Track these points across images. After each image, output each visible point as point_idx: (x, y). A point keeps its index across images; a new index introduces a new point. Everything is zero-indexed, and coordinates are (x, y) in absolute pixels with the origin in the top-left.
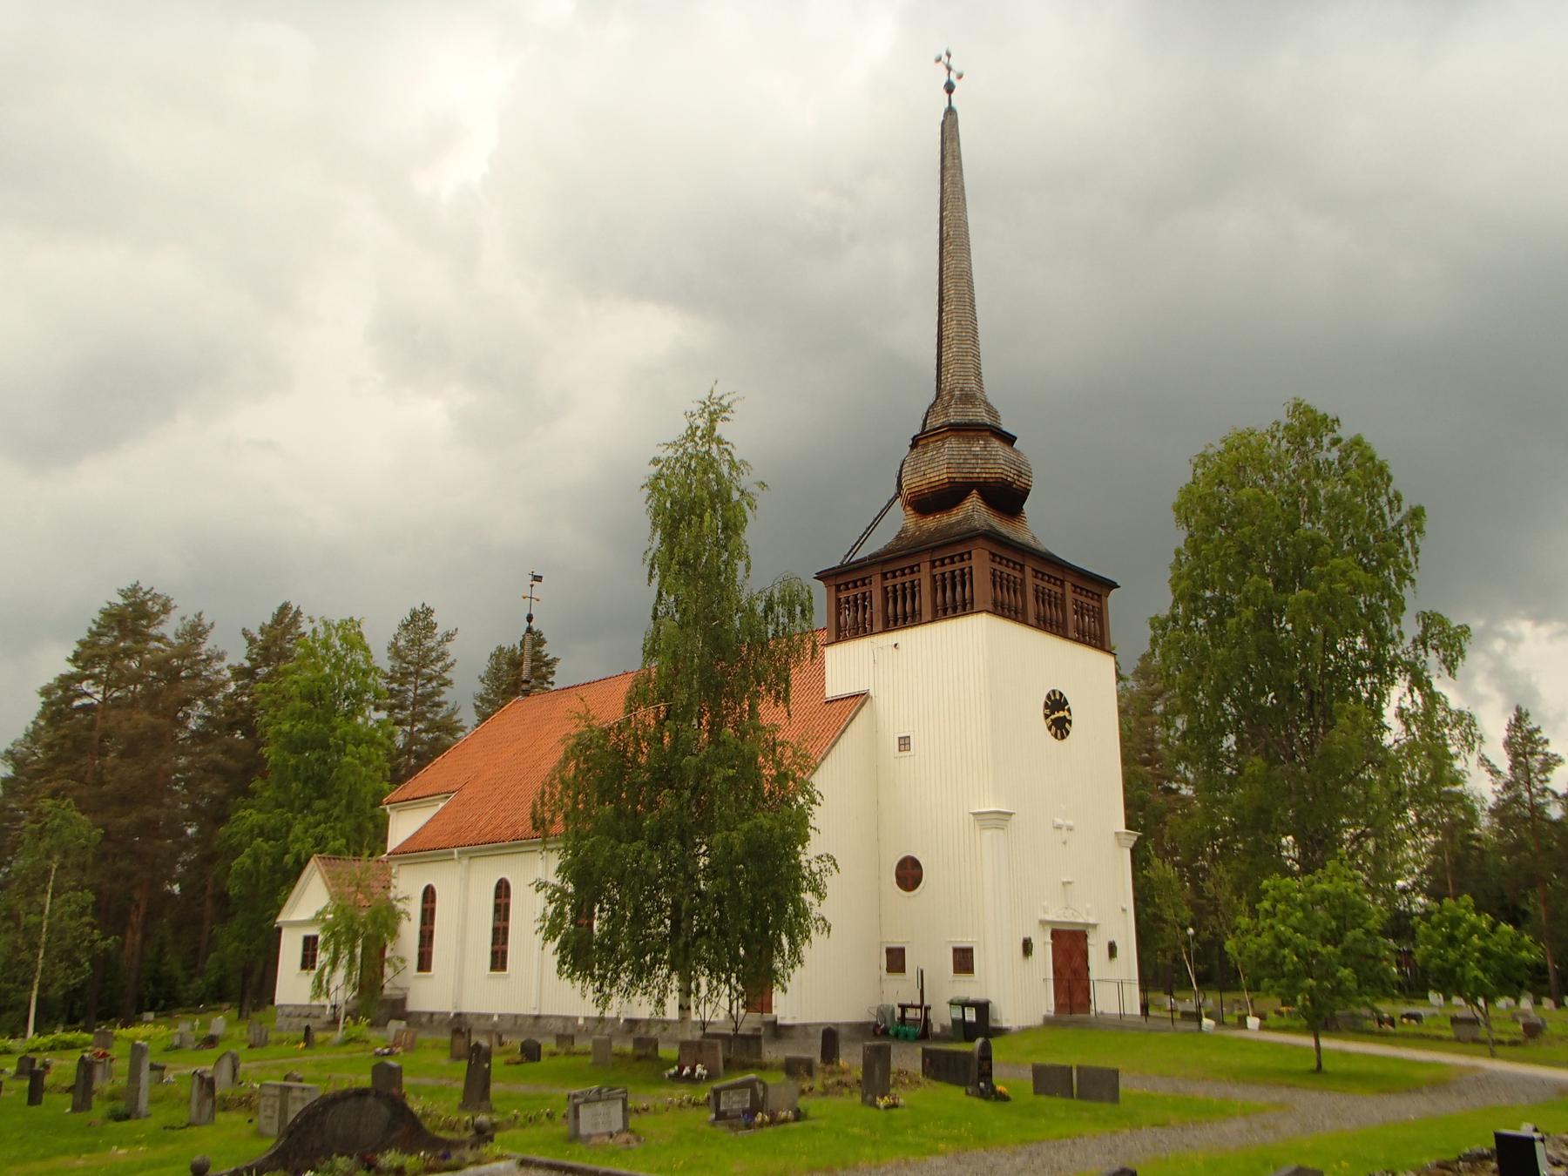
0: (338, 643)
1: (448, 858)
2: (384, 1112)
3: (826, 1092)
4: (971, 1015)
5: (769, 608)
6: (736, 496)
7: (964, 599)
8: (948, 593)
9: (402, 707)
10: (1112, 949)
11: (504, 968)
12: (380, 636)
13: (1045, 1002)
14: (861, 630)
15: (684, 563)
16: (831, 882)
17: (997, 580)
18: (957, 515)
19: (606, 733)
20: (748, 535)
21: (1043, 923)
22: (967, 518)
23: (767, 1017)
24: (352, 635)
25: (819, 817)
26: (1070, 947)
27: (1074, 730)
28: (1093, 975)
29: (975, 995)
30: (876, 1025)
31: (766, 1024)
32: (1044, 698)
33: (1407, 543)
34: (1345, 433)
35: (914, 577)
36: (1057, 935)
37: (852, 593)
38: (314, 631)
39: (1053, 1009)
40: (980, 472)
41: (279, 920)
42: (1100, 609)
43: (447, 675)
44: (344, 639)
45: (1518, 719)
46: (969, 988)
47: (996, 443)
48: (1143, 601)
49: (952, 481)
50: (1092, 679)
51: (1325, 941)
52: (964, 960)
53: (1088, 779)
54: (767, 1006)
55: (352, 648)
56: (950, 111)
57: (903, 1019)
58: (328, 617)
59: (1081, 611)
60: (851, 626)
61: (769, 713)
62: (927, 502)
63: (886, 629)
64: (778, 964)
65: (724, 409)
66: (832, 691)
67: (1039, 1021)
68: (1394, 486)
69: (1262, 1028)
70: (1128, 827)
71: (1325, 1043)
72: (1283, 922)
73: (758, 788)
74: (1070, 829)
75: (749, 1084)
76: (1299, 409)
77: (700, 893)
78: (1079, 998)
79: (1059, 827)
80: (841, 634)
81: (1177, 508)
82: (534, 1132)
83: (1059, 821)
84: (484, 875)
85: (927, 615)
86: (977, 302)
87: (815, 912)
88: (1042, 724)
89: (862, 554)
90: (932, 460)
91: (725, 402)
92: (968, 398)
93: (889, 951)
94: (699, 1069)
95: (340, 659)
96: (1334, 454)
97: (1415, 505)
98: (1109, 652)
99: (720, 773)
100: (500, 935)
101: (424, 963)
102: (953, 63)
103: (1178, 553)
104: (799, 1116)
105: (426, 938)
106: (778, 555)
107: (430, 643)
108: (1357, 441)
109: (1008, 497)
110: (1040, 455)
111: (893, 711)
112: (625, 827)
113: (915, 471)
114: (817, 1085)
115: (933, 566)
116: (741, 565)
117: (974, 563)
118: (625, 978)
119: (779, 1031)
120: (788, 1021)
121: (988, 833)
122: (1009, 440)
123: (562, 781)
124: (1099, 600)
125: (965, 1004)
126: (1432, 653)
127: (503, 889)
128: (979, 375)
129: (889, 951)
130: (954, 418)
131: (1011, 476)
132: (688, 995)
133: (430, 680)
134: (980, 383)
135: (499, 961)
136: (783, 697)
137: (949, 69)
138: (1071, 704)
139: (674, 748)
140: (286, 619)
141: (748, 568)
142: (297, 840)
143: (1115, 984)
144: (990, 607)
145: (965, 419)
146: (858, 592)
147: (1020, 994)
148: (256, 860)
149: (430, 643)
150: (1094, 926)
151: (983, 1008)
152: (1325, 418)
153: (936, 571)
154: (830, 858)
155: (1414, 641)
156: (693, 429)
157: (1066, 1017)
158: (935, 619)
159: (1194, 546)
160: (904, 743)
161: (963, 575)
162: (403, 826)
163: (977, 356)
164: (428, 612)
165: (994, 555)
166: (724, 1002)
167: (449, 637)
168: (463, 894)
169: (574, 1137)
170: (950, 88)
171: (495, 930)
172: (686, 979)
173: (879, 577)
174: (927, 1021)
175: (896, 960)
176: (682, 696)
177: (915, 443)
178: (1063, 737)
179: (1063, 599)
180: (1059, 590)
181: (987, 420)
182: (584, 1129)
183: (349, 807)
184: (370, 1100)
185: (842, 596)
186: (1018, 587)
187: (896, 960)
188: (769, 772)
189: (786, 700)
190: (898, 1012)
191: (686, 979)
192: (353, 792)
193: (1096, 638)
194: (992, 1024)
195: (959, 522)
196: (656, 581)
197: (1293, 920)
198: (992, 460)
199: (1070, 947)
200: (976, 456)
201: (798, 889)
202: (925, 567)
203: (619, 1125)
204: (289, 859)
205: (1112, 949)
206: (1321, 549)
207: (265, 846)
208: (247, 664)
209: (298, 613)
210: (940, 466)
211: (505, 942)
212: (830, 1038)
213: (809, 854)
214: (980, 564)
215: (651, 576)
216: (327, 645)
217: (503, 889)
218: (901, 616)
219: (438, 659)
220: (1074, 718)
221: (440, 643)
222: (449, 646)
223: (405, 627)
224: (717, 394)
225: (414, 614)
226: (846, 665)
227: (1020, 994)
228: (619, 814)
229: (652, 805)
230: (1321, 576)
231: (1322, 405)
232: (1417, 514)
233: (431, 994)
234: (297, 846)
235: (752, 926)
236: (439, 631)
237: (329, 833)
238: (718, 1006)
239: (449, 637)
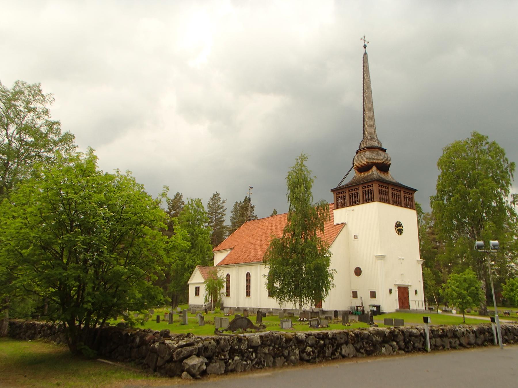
0: (195, 205)
1: (233, 266)
2: (246, 321)
3: (334, 323)
4: (375, 309)
5: (318, 207)
6: (309, 179)
8: (367, 196)
9: (212, 222)
10: (416, 292)
11: (250, 296)
12: (205, 202)
13: (396, 306)
14: (344, 205)
15: (297, 198)
16: (335, 276)
17: (380, 192)
18: (369, 173)
19: (279, 240)
20: (312, 190)
21: (395, 285)
22: (373, 174)
23: (321, 309)
24: (198, 203)
25: (331, 260)
26: (403, 292)
27: (404, 232)
28: (410, 299)
29: (376, 304)
30: (350, 312)
31: (321, 310)
32: (395, 224)
33: (509, 173)
34: (490, 140)
35: (357, 191)
36: (399, 288)
37: (340, 195)
38: (188, 202)
39: (398, 307)
40: (376, 161)
41: (189, 282)
42: (412, 197)
43: (224, 213)
44: (197, 204)
46: (375, 302)
47: (380, 152)
48: (425, 197)
49: (368, 164)
50: (409, 217)
51: (465, 290)
52: (373, 295)
53: (410, 243)
54: (321, 306)
55: (199, 206)
56: (365, 54)
57: (357, 310)
58: (192, 198)
59: (405, 198)
60: (341, 204)
61: (319, 234)
62: (362, 169)
63: (350, 206)
64: (323, 295)
65: (305, 158)
67: (394, 311)
68: (506, 156)
69: (457, 313)
70: (420, 258)
71: (466, 316)
72: (453, 285)
73: (316, 253)
74: (403, 259)
75: (317, 320)
76: (475, 134)
77: (304, 278)
78: (406, 305)
79: (400, 259)
80: (337, 207)
81: (438, 164)
82: (273, 327)
83: (400, 257)
84: (243, 271)
85: (361, 202)
86: (341, 233)
87: (332, 282)
88: (395, 231)
89: (344, 184)
90: (362, 157)
91: (305, 156)
92: (372, 139)
93: (353, 292)
94: (305, 319)
95: (196, 210)
96: (487, 146)
99: (308, 250)
100: (248, 287)
101: (228, 295)
102: (366, 39)
103: (439, 177)
104: (328, 326)
106: (320, 193)
107: (219, 203)
108: (494, 143)
109: (384, 167)
110: (394, 154)
111: (352, 228)
112: (285, 262)
113: (357, 161)
114: (333, 322)
115: (363, 188)
116: (311, 198)
117: (374, 187)
118: (287, 298)
119: (324, 312)
120: (326, 310)
121: (379, 261)
122: (384, 150)
123: (270, 252)
124: (412, 195)
125: (373, 306)
127: (248, 275)
128: (375, 132)
129: (353, 292)
130: (368, 145)
131: (385, 161)
132: (301, 302)
133: (219, 214)
134: (376, 134)
135: (248, 294)
136: (322, 230)
137: (365, 41)
138: (403, 225)
139: (296, 243)
140: (178, 197)
141: (312, 199)
142: (188, 260)
143: (417, 301)
144: (379, 200)
146: (342, 195)
147: (389, 304)
148: (177, 266)
149: (219, 203)
150: (411, 286)
151: (378, 307)
152: (483, 136)
154: (335, 270)
155: (511, 203)
156: (298, 163)
157: (402, 310)
158: (363, 203)
159: (444, 174)
160: (356, 237)
161: (371, 191)
162: (219, 258)
163: (374, 126)
164: (218, 194)
166: (310, 304)
167: (224, 202)
168: (237, 276)
169: (282, 328)
170: (365, 47)
171: (247, 286)
172: (301, 298)
174: (363, 310)
175: (355, 294)
176: (297, 231)
177: (357, 152)
179: (400, 195)
180: (399, 193)
181: (378, 145)
182: (284, 327)
183: (201, 251)
184: (244, 319)
185: (338, 196)
186: (387, 193)
187: (355, 294)
188: (319, 248)
189: (323, 231)
190: (356, 308)
191: (301, 298)
192: (202, 247)
193: (410, 205)
194: (381, 311)
195: (370, 175)
196: (289, 202)
197: (456, 285)
198: (379, 157)
199: (403, 292)
200: (374, 156)
201: (327, 277)
203: (290, 326)
204: (186, 266)
205: (416, 292)
206: (481, 176)
207: (179, 262)
208: (168, 210)
209: (181, 195)
210: (364, 159)
211: (250, 289)
212: (336, 313)
213: (329, 269)
214: (376, 188)
215: (288, 201)
216: (192, 206)
217: (248, 275)
218: (354, 202)
219: (222, 208)
220: (404, 229)
221: (222, 203)
222: (224, 204)
223: (212, 199)
224: (303, 154)
225: (214, 195)
226: (339, 215)
227: (389, 304)
228: (283, 259)
229: (291, 257)
230: (480, 185)
231: (482, 133)
232: (512, 164)
233: (230, 302)
234: (188, 262)
235: (316, 286)
236: (221, 200)
237: (196, 259)
238: (308, 306)
239: (224, 202)
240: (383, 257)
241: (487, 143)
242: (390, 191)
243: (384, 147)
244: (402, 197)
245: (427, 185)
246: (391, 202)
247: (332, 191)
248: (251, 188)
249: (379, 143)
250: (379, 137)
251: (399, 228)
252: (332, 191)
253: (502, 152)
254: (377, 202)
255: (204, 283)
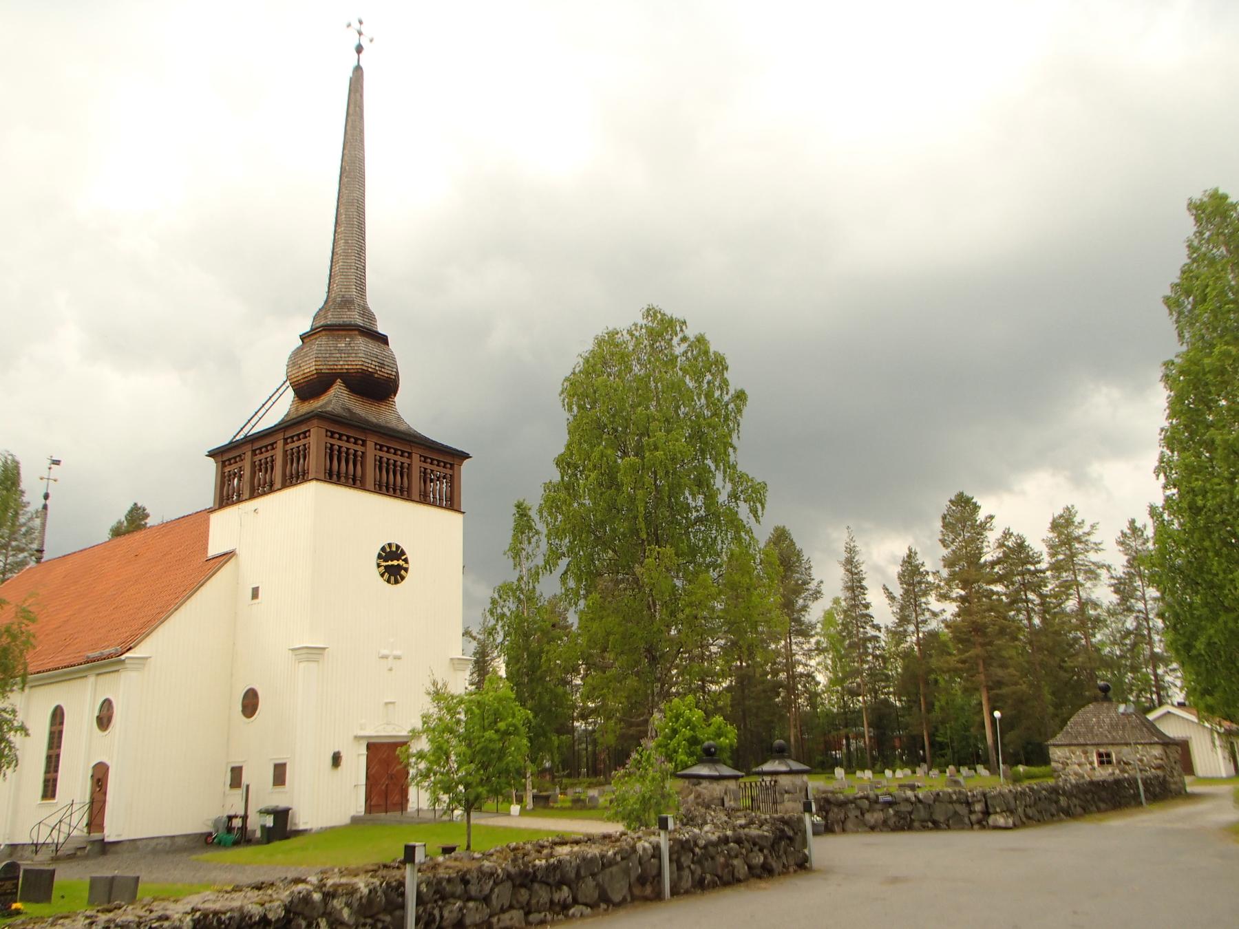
7: (298, 472)
27: (409, 577)
32: (378, 550)
39: (363, 809)
45: (909, 556)
46: (278, 799)
49: (319, 374)
52: (280, 774)
56: (358, 70)
66: (213, 551)
67: (347, 820)
74: (398, 658)
76: (651, 313)
79: (385, 657)
97: (739, 388)
98: (459, 511)
105: (53, 763)
109: (378, 386)
111: (248, 569)
115: (286, 443)
121: (302, 665)
122: (383, 340)
126: (741, 503)
129: (233, 769)
138: (409, 555)
145: (341, 321)
153: (289, 447)
158: (284, 486)
160: (255, 593)
165: (333, 433)
170: (359, 49)
173: (250, 453)
178: (396, 582)
181: (360, 322)
185: (226, 470)
198: (359, 354)
200: (340, 351)
202: (280, 444)
220: (411, 566)
240: (314, 653)
241: (684, 339)
242: (371, 452)
243: (381, 329)
244: (416, 474)
245: (522, 451)
246: (415, 495)
247: (212, 454)
248: (57, 462)
249: (370, 317)
250: (372, 303)
251: (393, 564)
252: (212, 454)
253: (719, 364)
254: (314, 483)
255: (1228, 779)
